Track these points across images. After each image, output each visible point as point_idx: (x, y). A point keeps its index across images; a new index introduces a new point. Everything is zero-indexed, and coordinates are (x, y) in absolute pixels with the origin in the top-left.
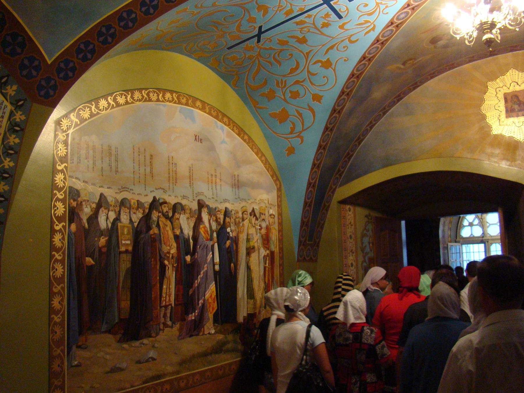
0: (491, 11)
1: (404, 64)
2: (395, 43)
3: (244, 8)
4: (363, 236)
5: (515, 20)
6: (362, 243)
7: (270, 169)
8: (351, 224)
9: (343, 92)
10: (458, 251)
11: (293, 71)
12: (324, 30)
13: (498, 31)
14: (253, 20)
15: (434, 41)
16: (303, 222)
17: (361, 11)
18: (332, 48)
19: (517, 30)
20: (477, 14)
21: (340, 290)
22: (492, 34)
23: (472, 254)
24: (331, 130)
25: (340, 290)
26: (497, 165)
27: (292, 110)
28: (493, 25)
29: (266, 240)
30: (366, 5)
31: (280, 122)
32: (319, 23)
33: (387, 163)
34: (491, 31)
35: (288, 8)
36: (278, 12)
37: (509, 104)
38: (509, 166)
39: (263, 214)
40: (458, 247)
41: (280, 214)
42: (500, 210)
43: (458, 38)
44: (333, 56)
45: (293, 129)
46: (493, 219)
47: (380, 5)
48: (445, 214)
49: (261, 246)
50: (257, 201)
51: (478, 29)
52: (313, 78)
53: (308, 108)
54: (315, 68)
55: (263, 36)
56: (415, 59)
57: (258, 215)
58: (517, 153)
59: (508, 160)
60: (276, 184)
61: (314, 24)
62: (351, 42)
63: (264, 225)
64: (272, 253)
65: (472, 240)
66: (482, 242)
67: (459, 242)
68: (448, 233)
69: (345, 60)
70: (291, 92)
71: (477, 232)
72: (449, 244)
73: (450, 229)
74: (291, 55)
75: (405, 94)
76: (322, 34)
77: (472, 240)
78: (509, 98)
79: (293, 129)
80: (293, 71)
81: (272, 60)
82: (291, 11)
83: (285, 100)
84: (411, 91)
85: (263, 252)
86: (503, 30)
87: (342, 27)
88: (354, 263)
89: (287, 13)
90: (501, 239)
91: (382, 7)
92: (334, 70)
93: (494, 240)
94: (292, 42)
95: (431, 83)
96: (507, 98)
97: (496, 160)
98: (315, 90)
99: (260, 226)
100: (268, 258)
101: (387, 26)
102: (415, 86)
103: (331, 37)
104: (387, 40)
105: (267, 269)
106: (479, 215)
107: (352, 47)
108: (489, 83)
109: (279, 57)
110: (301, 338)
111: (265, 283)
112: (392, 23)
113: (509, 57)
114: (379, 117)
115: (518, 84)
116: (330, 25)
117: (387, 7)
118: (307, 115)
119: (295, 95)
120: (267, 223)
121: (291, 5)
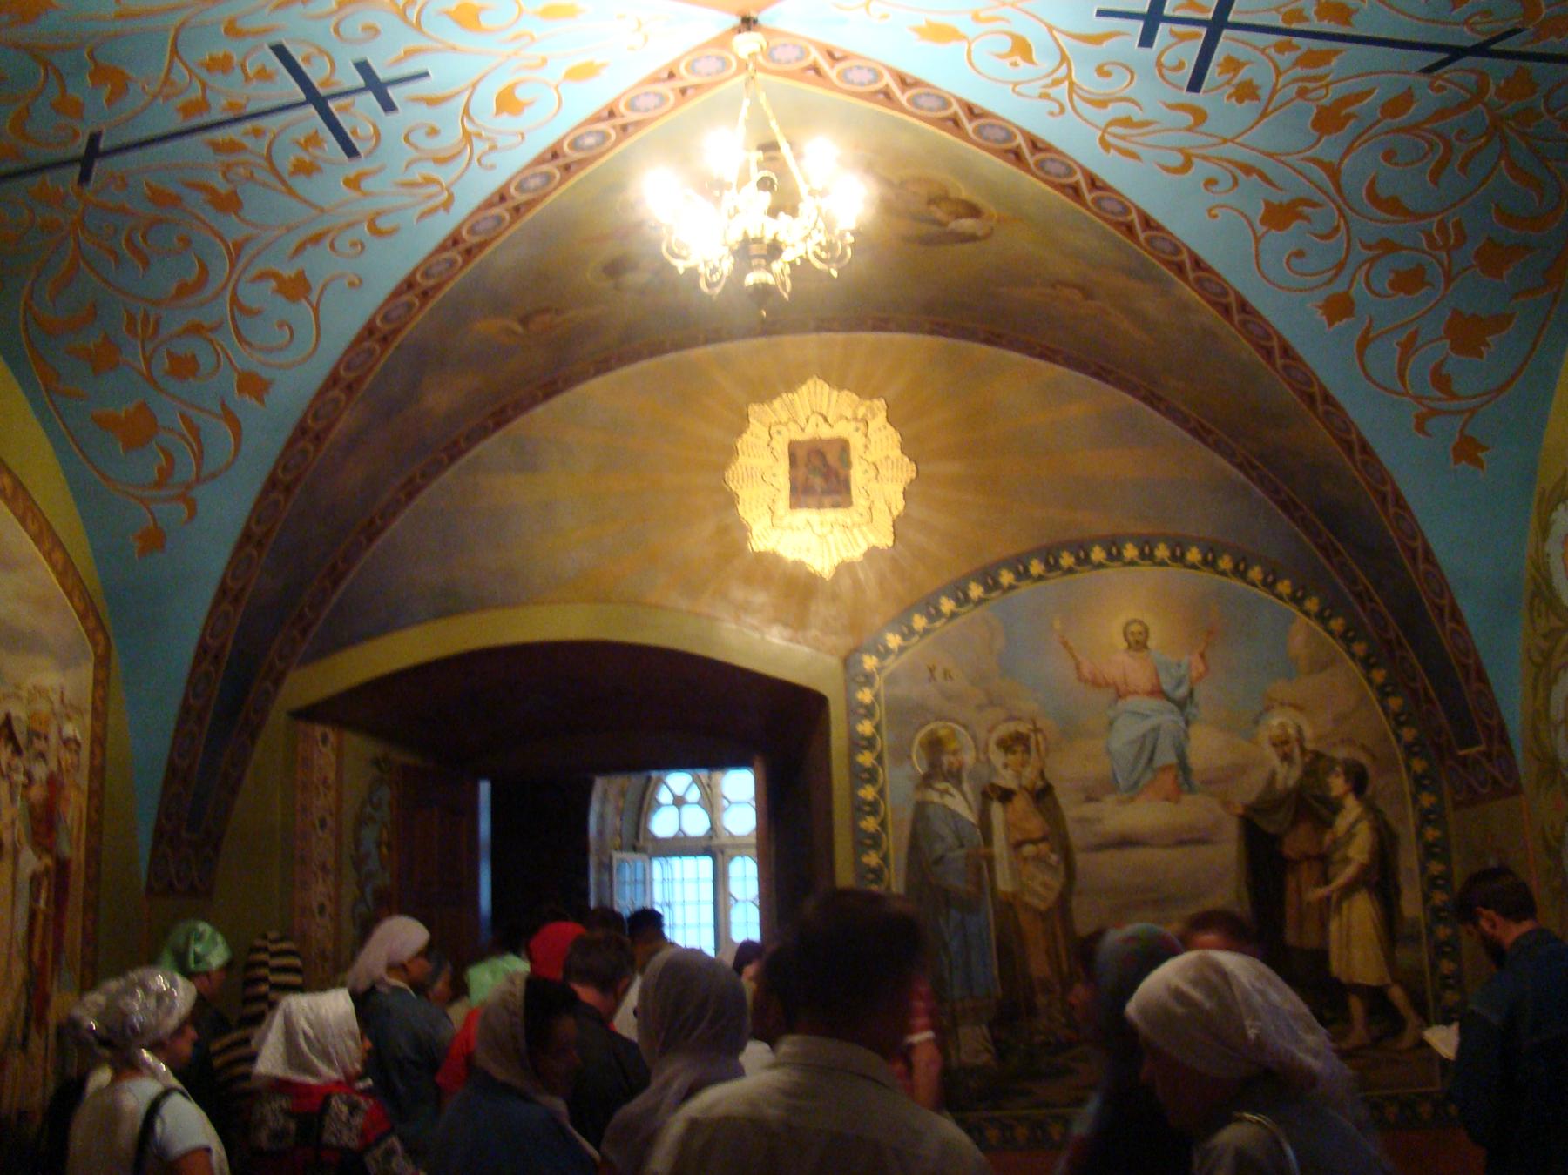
0: (773, 213)
1: (524, 321)
2: (503, 257)
3: (47, 65)
4: (361, 822)
5: (830, 247)
6: (357, 843)
7: (77, 593)
8: (334, 782)
9: (333, 379)
10: (640, 876)
11: (184, 290)
12: (300, 183)
13: (788, 270)
14: (78, 110)
15: (615, 269)
16: (172, 770)
17: (416, 148)
18: (316, 239)
19: (835, 273)
20: (737, 211)
21: (264, 988)
22: (770, 271)
23: (677, 886)
24: (288, 489)
25: (264, 988)
26: (757, 636)
28: (775, 250)
29: (44, 823)
30: (433, 132)
31: (128, 446)
32: (286, 159)
33: (449, 604)
34: (769, 263)
35: (195, 93)
36: (160, 100)
37: (802, 472)
38: (791, 640)
39: (38, 736)
40: (639, 864)
41: (98, 741)
42: (757, 763)
43: (681, 271)
44: (319, 265)
45: (166, 474)
46: (739, 787)
47: (475, 140)
48: (608, 769)
49: (24, 840)
50: (24, 694)
51: (734, 253)
52: (245, 323)
53: (219, 410)
54: (257, 295)
55: (98, 165)
56: (558, 312)
57: (21, 738)
58: (813, 608)
59: (786, 625)
60: (94, 643)
61: (269, 158)
62: (376, 232)
63: (40, 771)
64: (62, 866)
65: (681, 846)
66: (707, 851)
68: (613, 821)
69: (352, 284)
70: (171, 355)
71: (696, 823)
72: (617, 856)
73: (620, 813)
74: (187, 242)
75: (523, 406)
76: (291, 192)
77: (681, 846)
78: (801, 454)
79: (166, 474)
80: (184, 290)
81: (124, 249)
82: (202, 105)
83: (150, 379)
84: (534, 402)
85: (30, 862)
86: (801, 270)
87: (354, 183)
88: (327, 903)
89: (187, 110)
90: (758, 847)
91: (480, 147)
92: (316, 310)
93: (738, 847)
94: (195, 200)
95: (596, 388)
96: (796, 454)
97: (755, 622)
98: (247, 360)
99: (29, 775)
100: (45, 883)
101: (488, 204)
102: (550, 389)
103: (312, 205)
104: (482, 246)
105: (41, 918)
106: (703, 774)
107: (374, 244)
108: (754, 409)
109: (144, 237)
111: (30, 963)
112: (502, 196)
113: (810, 345)
114: (437, 468)
115: (826, 420)
116: (319, 169)
117: (493, 148)
118: (218, 435)
119: (184, 367)
120: (54, 766)
121: (204, 86)
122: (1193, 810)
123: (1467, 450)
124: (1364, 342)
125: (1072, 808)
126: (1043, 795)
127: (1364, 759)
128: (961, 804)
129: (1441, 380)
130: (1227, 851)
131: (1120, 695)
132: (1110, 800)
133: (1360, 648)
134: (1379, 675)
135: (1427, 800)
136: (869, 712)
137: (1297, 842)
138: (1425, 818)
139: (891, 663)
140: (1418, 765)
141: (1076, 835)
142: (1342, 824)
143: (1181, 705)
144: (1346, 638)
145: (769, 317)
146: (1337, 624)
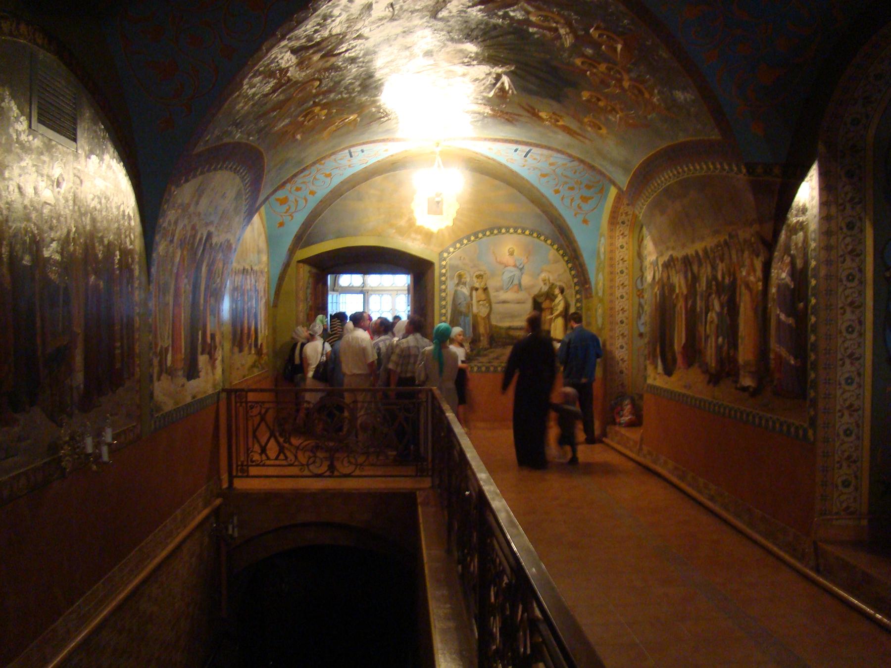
4: (307, 288)
27: (292, 198)
33: (339, 235)
44: (334, 172)
66: (361, 292)
67: (337, 291)
110: (320, 349)
118: (302, 202)
119: (298, 189)
122: (522, 295)
123: (585, 221)
124: (562, 199)
127: (564, 285)
129: (580, 208)
130: (529, 306)
131: (506, 266)
132: (502, 292)
133: (566, 258)
134: (570, 265)
135: (578, 296)
137: (545, 305)
138: (577, 301)
140: (577, 288)
142: (557, 301)
143: (521, 269)
144: (563, 256)
146: (561, 252)
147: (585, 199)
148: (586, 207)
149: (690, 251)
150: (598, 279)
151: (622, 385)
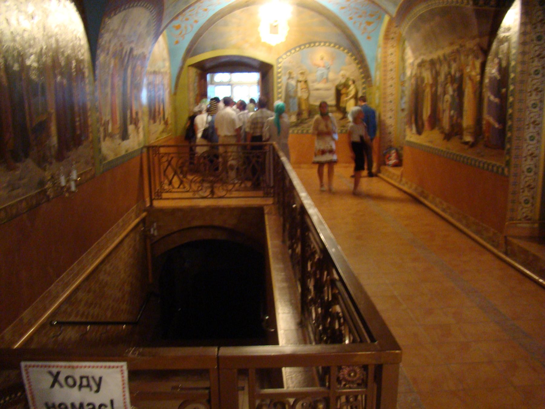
79: (181, 33)
118: (189, 29)
119: (187, 19)
122: (328, 85)
123: (369, 38)
125: (310, 84)
126: (306, 82)
128: (293, 82)
130: (333, 92)
136: (280, 68)
137: (343, 91)
139: (285, 60)
141: (311, 88)
145: (264, 45)
147: (369, 23)
148: (370, 28)
149: (434, 56)
150: (376, 74)
151: (390, 141)
